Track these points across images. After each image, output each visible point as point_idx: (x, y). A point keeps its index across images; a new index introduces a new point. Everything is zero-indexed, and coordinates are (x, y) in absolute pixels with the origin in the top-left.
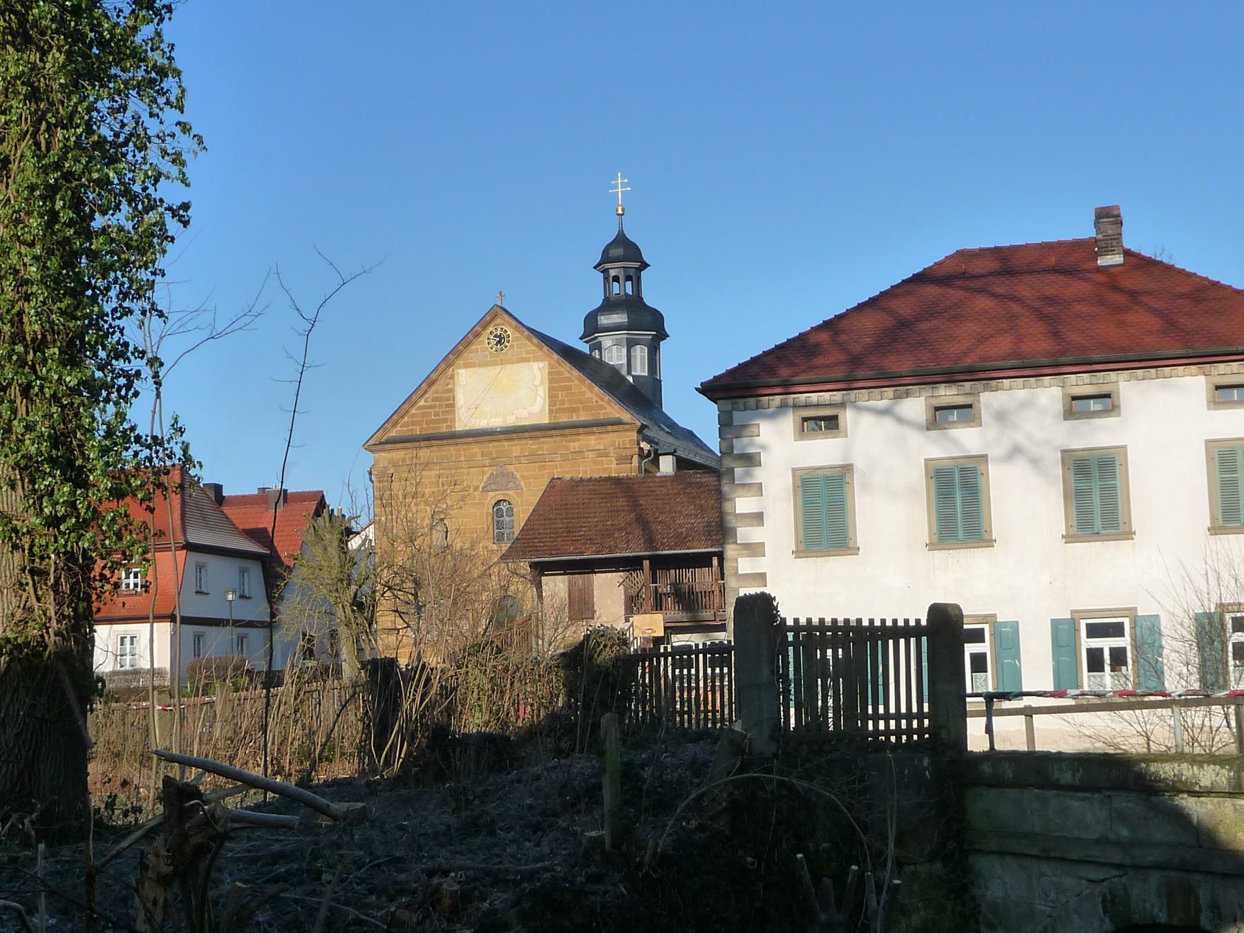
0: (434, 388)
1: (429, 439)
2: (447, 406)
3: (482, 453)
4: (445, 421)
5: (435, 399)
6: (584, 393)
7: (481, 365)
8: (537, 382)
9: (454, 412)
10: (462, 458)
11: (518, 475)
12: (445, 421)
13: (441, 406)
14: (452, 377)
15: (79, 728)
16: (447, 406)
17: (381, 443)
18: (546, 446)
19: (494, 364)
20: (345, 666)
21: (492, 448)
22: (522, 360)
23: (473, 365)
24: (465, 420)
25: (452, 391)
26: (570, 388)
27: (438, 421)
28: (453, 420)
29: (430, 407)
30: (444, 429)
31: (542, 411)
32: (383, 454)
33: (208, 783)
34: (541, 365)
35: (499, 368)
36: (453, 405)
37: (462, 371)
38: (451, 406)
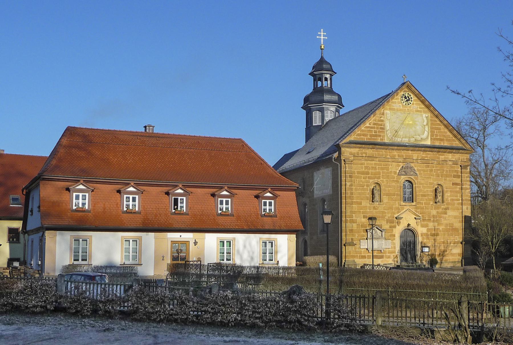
3: (399, 155)
4: (380, 136)
5: (374, 124)
8: (425, 123)
10: (388, 157)
11: (416, 168)
12: (380, 136)
21: (404, 153)
26: (440, 129)
29: (372, 128)
30: (379, 140)
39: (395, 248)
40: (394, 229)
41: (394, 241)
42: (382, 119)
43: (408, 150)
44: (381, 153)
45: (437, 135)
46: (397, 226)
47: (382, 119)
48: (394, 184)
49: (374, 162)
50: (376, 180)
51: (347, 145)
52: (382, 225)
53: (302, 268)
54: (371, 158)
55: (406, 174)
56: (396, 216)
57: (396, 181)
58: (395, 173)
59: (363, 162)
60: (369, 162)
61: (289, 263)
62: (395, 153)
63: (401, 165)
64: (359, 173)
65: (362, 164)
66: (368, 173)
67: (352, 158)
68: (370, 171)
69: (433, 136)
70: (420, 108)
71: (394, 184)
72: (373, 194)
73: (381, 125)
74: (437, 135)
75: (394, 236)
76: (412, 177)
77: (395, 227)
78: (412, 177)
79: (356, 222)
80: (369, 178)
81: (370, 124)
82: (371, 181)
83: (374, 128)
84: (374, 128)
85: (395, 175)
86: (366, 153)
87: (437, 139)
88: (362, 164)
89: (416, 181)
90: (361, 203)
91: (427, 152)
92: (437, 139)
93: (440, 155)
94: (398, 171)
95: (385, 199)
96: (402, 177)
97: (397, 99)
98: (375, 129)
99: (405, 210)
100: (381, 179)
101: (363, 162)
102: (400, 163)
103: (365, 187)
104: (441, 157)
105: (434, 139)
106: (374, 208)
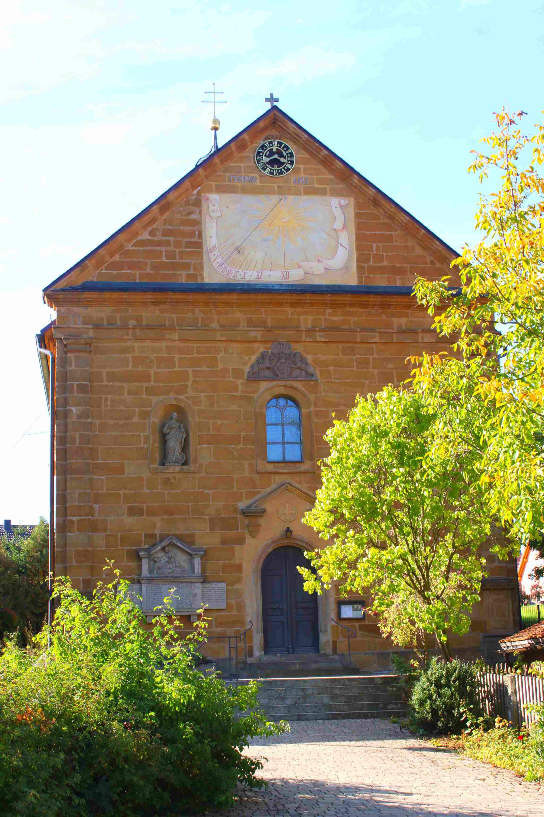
0: (166, 215)
1: (160, 289)
2: (190, 244)
3: (250, 322)
4: (186, 266)
5: (167, 233)
6: (413, 248)
7: (245, 191)
8: (339, 224)
9: (200, 255)
10: (215, 325)
11: (310, 358)
12: (186, 266)
13: (178, 244)
14: (198, 203)
15: (42, 623)
16: (190, 244)
17: (74, 289)
18: (353, 319)
19: (269, 192)
20: (248, 603)
21: (268, 315)
22: (311, 191)
23: (232, 190)
24: (217, 269)
25: (198, 223)
26: (390, 239)
27: (174, 267)
28: (200, 267)
29: (159, 244)
30: (182, 278)
31: (346, 268)
32: (75, 309)
33: (423, 806)
34: (343, 202)
35: (275, 198)
36: (199, 245)
37: (214, 197)
38: (196, 245)
39: (241, 607)
40: (237, 547)
41: (237, 586)
42: (193, 217)
43: (281, 304)
44: (189, 315)
45: (379, 258)
46: (249, 540)
47: (193, 217)
48: (234, 407)
49: (164, 344)
50: (171, 399)
51: (70, 295)
52: (193, 535)
53: (231, 534)
54: (159, 329)
55: (276, 377)
56: (242, 505)
57: (242, 398)
58: (238, 373)
59: (129, 344)
60: (148, 343)
61: (360, 281)
62: (239, 315)
63: (261, 349)
64: (112, 377)
65: (125, 350)
66: (146, 378)
67: (91, 334)
68: (152, 372)
69: (367, 261)
70: (320, 181)
71: (234, 407)
72: (164, 440)
73: (192, 234)
74: (379, 258)
75: (239, 568)
76: (298, 385)
77: (241, 541)
78: (298, 385)
79: (105, 530)
80: (150, 391)
81: (152, 233)
82: (155, 399)
83: (168, 243)
84: (168, 243)
85: (239, 382)
86: (139, 319)
87: (382, 270)
88: (125, 350)
89: (312, 397)
90: (120, 469)
91: (348, 309)
92: (382, 270)
93: (393, 315)
94: (247, 369)
95: (204, 454)
96: (264, 385)
97: (242, 159)
98: (171, 249)
99: (273, 486)
100: (191, 392)
101: (129, 344)
102: (255, 345)
103: (136, 419)
104: (395, 320)
105: (372, 270)
106: (167, 482)
